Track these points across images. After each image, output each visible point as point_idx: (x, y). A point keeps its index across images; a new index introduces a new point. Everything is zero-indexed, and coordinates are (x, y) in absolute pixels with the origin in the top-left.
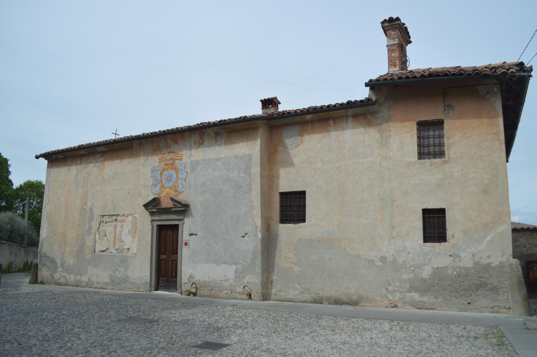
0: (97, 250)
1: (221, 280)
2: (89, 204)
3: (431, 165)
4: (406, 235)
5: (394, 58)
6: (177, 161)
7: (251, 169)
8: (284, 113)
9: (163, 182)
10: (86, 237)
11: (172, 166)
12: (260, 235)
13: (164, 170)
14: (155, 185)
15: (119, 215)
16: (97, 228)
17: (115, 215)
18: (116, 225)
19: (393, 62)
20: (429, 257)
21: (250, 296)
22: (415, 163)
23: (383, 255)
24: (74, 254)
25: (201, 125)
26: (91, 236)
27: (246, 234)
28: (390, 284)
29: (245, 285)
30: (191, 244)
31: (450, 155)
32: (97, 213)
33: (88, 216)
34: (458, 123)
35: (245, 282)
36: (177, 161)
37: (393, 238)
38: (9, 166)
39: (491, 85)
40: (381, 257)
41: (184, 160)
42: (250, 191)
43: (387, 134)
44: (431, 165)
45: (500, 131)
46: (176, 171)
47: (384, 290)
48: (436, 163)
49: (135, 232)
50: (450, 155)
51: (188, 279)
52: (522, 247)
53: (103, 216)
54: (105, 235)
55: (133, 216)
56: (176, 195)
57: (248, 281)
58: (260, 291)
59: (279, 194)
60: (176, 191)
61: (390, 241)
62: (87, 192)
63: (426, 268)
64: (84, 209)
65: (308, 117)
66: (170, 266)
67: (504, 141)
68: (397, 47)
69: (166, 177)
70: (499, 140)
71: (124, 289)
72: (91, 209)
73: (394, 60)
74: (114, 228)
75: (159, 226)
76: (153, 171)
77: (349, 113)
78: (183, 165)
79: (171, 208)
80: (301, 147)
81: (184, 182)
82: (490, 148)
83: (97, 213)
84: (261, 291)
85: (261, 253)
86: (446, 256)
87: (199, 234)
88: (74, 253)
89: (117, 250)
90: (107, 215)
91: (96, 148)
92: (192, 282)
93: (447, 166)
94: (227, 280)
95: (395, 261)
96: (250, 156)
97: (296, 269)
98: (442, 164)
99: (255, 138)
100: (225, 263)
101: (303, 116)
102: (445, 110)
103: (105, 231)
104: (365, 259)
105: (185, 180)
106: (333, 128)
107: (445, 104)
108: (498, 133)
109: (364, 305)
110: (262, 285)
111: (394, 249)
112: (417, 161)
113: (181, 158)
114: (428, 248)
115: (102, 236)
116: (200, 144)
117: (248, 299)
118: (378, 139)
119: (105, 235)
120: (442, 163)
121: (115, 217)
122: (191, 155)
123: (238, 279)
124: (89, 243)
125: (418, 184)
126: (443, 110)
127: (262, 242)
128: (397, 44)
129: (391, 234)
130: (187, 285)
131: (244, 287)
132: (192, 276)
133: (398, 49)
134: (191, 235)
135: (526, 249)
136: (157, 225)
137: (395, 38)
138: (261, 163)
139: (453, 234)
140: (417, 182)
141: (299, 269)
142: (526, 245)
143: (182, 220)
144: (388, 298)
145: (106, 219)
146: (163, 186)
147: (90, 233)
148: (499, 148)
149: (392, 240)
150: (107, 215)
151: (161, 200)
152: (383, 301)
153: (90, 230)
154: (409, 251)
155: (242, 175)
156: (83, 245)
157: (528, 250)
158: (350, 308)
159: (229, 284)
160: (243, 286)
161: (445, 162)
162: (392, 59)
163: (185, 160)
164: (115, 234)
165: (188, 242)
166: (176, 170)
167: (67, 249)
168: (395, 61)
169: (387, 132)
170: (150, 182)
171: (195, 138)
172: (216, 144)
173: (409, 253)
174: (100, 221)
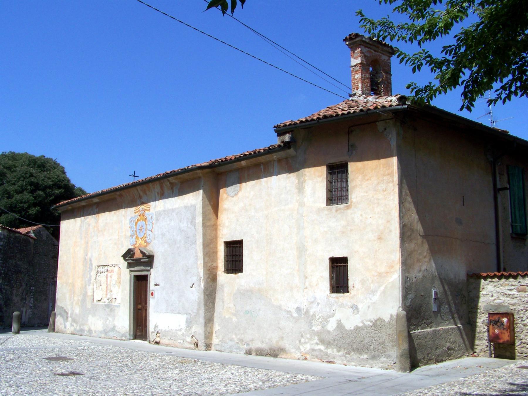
0: (95, 300)
1: (176, 330)
2: (89, 255)
3: (337, 211)
4: (316, 285)
5: (357, 80)
6: (146, 212)
7: (195, 220)
8: (434, 109)
9: (137, 233)
10: (88, 286)
11: (143, 217)
12: (202, 285)
13: (138, 220)
14: (132, 236)
15: (109, 265)
16: (95, 278)
17: (106, 265)
18: (107, 274)
19: (356, 85)
20: (334, 308)
21: (196, 345)
22: (323, 209)
23: (299, 306)
24: (80, 304)
25: (159, 176)
26: (91, 286)
27: (193, 284)
28: (302, 336)
29: (193, 334)
30: (156, 294)
31: (353, 199)
32: (95, 263)
33: (89, 266)
34: (359, 164)
35: (193, 332)
36: (146, 212)
37: (306, 288)
38: (481, 123)
39: (388, 121)
40: (297, 308)
41: (151, 211)
42: (195, 241)
43: (303, 179)
44: (337, 211)
45: (394, 171)
46: (145, 222)
47: (298, 342)
48: (340, 209)
49: (120, 282)
50: (353, 199)
51: (154, 329)
52: (489, 296)
53: (99, 266)
54: (101, 285)
55: (118, 266)
56: (146, 246)
57: (195, 331)
58: (203, 341)
59: (223, 243)
60: (146, 241)
61: (304, 291)
62: (88, 243)
63: (331, 319)
64: (86, 259)
65: (243, 163)
66: (144, 316)
67: (397, 182)
68: (360, 67)
69: (139, 228)
70: (393, 181)
71: (113, 338)
72: (91, 260)
73: (357, 83)
74: (106, 278)
75: (135, 276)
76: (131, 222)
77: (274, 158)
78: (151, 216)
79: (141, 259)
80: (240, 194)
81: (150, 233)
82: (385, 190)
83: (95, 263)
84: (204, 340)
85: (203, 303)
86: (347, 307)
87: (161, 285)
88: (79, 302)
89: (108, 299)
90: (101, 266)
91: (91, 199)
92: (156, 332)
93: (349, 211)
94: (180, 330)
95: (307, 312)
96: (194, 206)
97: (234, 319)
98: (345, 210)
99: (199, 189)
100: (179, 313)
101: (239, 163)
102: (349, 151)
103: (100, 281)
104: (285, 310)
105: (151, 230)
106: (263, 173)
107: (350, 143)
108: (391, 174)
109: (282, 357)
110: (205, 334)
111: (307, 299)
112: (326, 207)
113: (149, 209)
114: (333, 299)
115: (98, 286)
116: (162, 196)
117: (195, 348)
118: (296, 184)
119: (101, 285)
120: (346, 208)
121: (106, 268)
122: (155, 206)
123: (188, 329)
124: (90, 293)
125: (326, 232)
126: (348, 150)
127: (205, 293)
128: (359, 64)
129: (305, 285)
130: (153, 334)
131: (193, 336)
132: (157, 325)
133: (360, 69)
134: (156, 285)
135: (492, 298)
136: (134, 275)
137: (358, 57)
138: (203, 213)
139: (353, 284)
140: (326, 229)
141: (236, 320)
142: (493, 293)
143: (149, 271)
144: (300, 349)
145: (101, 269)
146: (137, 237)
147: (90, 283)
148: (393, 190)
149: (306, 290)
150: (101, 266)
151: (136, 251)
152: (297, 353)
153: (90, 280)
154: (318, 302)
155: (189, 225)
156: (85, 295)
157: (495, 299)
158: (272, 359)
159: (182, 334)
160: (191, 336)
161: (348, 208)
162: (355, 81)
163: (152, 211)
164: (107, 284)
165: (153, 292)
166: (145, 220)
167: (75, 298)
168: (358, 84)
169: (303, 177)
170: (129, 234)
171: (157, 187)
172: (172, 194)
173: (318, 304)
174: (97, 271)
